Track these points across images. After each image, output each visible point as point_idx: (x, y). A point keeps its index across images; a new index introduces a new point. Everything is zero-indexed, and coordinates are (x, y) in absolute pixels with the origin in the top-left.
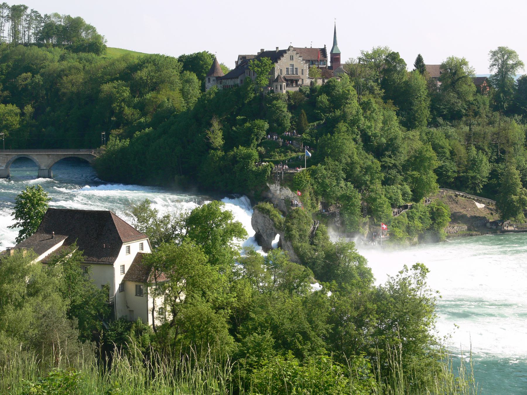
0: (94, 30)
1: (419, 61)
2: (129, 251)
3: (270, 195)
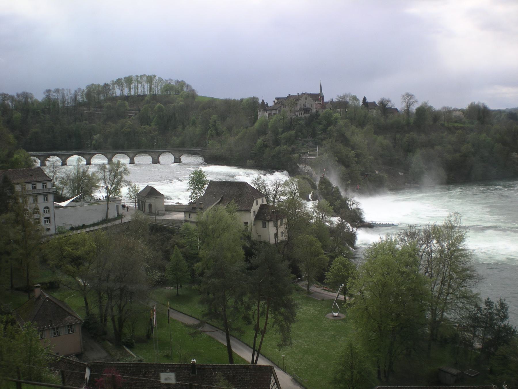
0: (191, 87)
1: (365, 99)
2: (257, 204)
3: (299, 170)
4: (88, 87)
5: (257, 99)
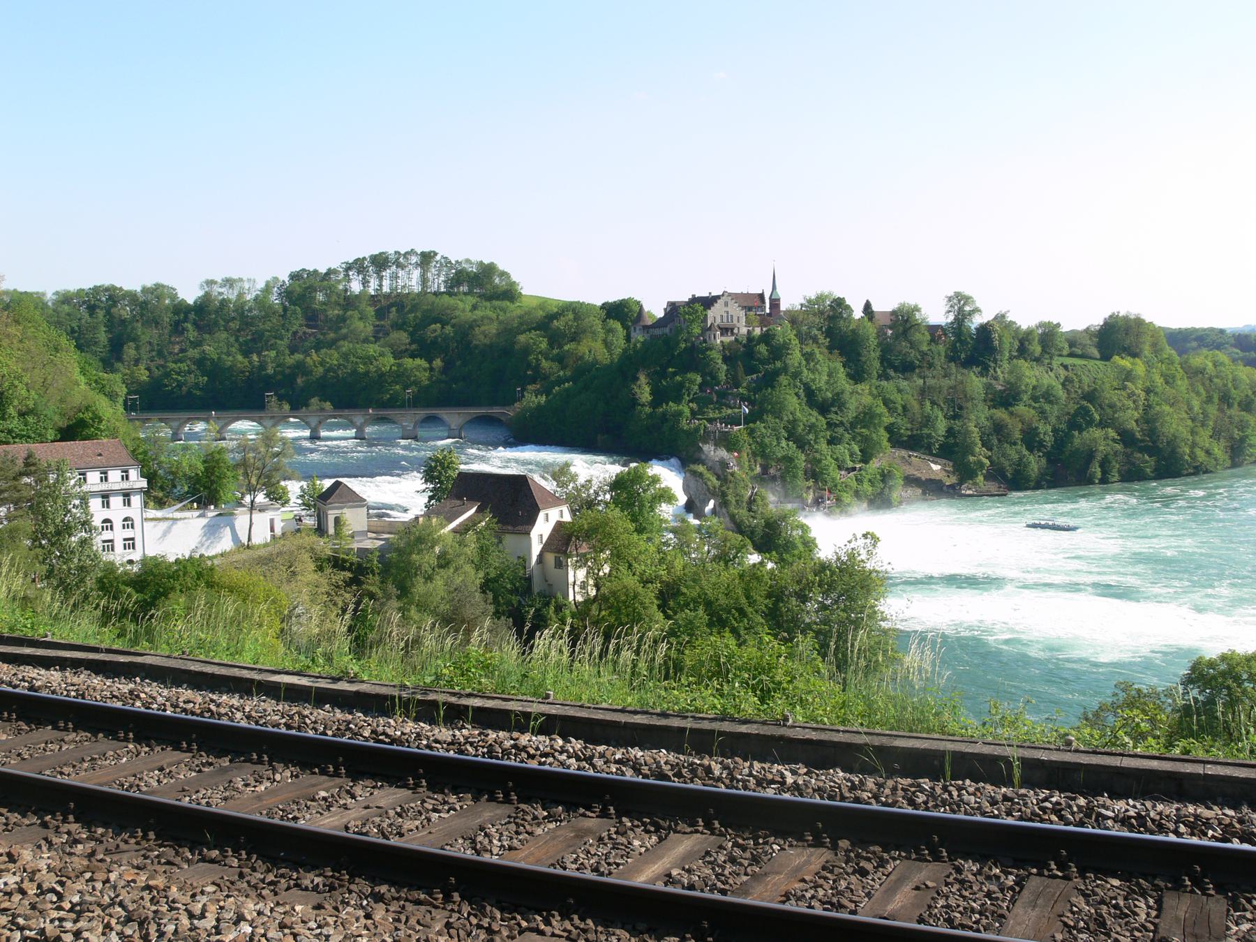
1: (868, 306)
4: (295, 276)
5: (839, 303)
